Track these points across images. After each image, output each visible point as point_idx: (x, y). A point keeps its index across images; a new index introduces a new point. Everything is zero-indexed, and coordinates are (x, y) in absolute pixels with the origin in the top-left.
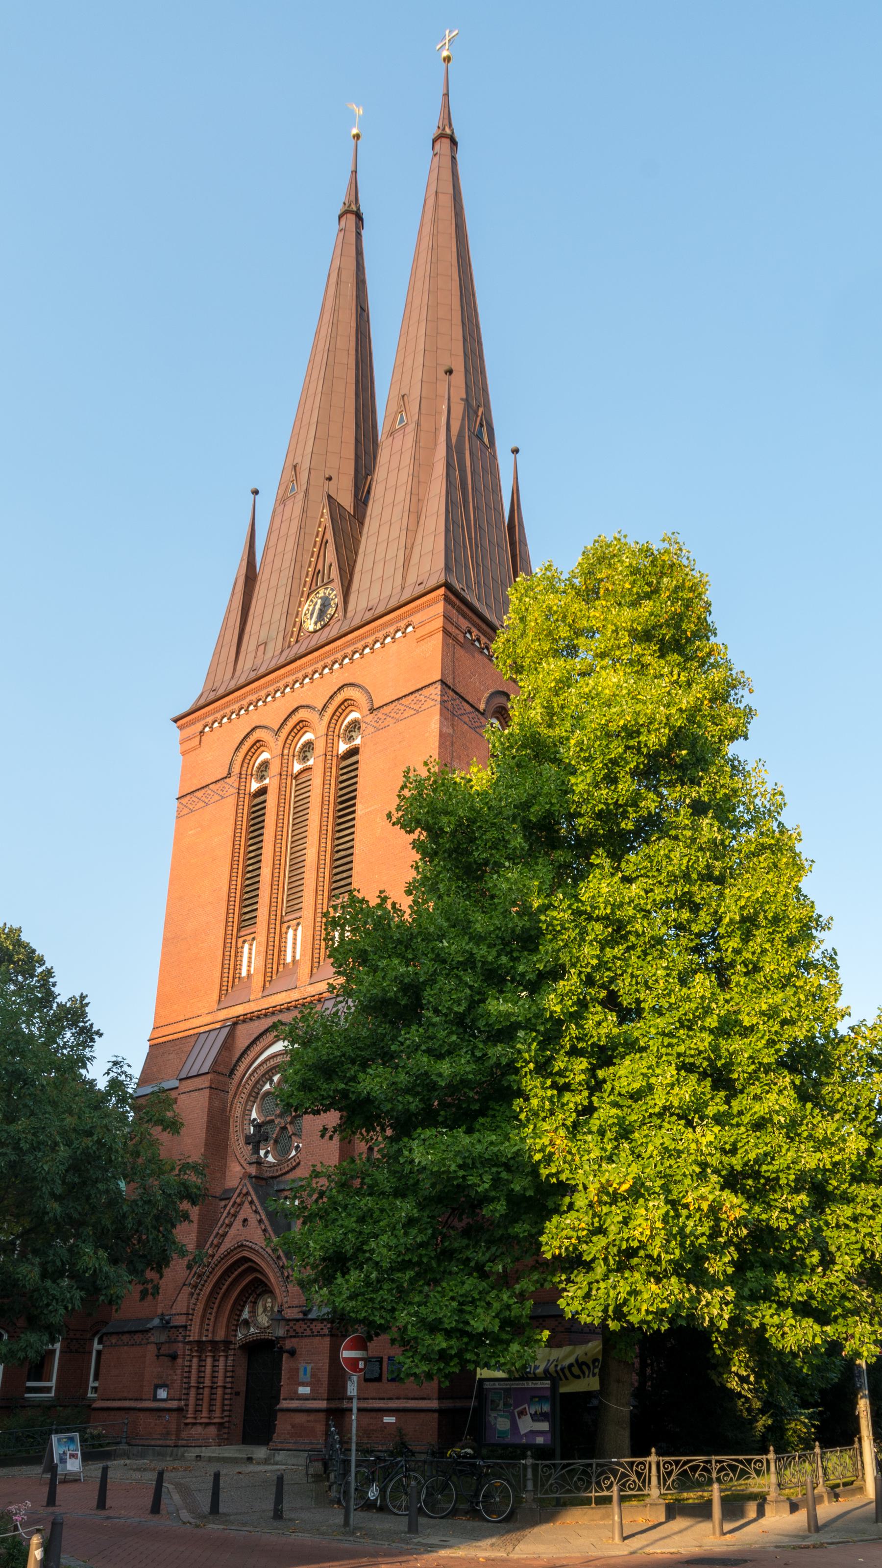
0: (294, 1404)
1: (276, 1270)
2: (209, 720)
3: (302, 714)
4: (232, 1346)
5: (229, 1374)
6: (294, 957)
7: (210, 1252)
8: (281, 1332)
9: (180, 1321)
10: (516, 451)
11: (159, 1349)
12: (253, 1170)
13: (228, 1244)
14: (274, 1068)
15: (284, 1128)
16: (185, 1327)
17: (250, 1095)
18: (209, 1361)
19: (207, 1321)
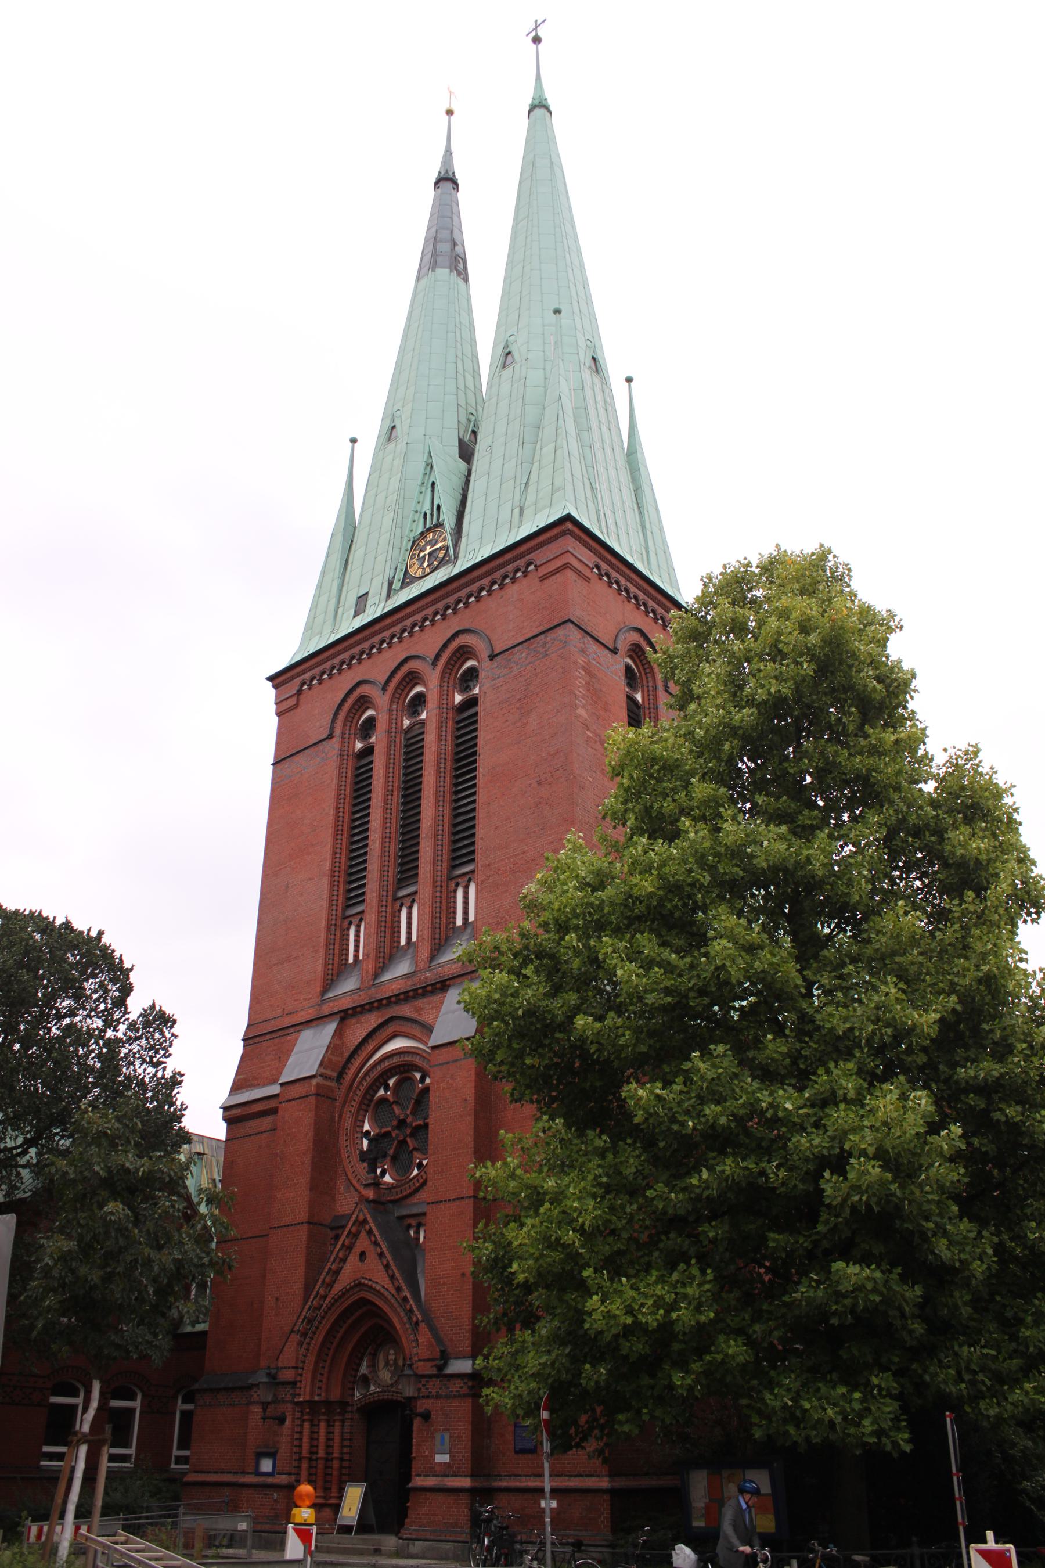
0: (431, 1482)
1: (403, 1314)
2: (307, 676)
3: (412, 665)
4: (350, 1408)
5: (347, 1443)
6: (356, 956)
7: (322, 1292)
8: (409, 1391)
9: (288, 1375)
10: (629, 380)
11: (264, 1410)
12: (370, 1194)
13: (345, 1280)
14: (395, 1068)
15: (403, 1143)
16: (294, 1383)
17: (361, 1103)
18: (323, 1425)
19: (319, 1377)
